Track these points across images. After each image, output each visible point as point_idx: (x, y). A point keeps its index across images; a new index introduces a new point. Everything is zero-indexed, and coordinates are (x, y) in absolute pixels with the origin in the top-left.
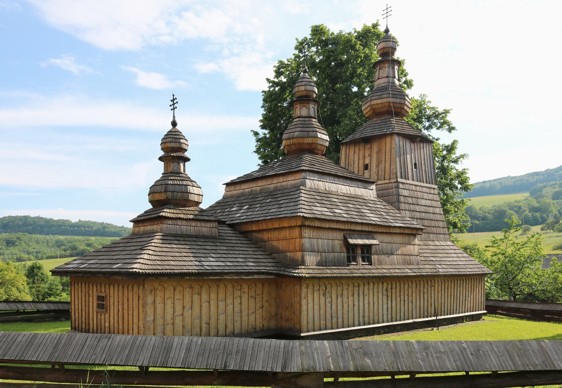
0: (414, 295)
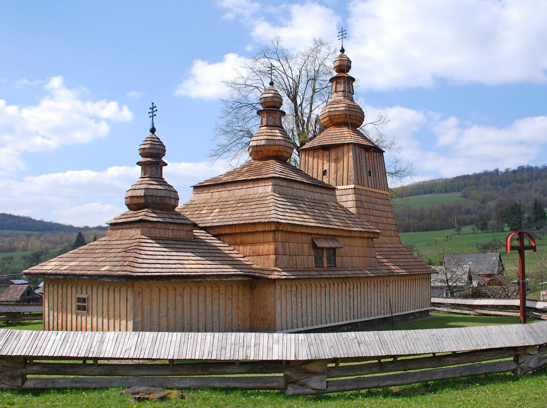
0: (372, 294)
